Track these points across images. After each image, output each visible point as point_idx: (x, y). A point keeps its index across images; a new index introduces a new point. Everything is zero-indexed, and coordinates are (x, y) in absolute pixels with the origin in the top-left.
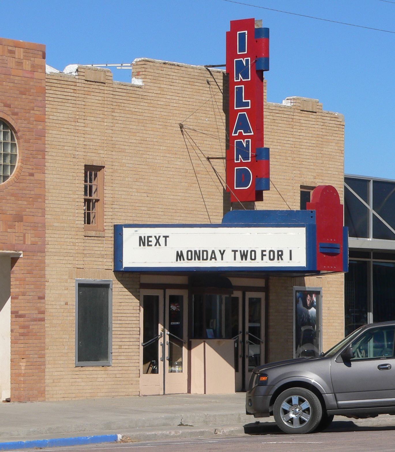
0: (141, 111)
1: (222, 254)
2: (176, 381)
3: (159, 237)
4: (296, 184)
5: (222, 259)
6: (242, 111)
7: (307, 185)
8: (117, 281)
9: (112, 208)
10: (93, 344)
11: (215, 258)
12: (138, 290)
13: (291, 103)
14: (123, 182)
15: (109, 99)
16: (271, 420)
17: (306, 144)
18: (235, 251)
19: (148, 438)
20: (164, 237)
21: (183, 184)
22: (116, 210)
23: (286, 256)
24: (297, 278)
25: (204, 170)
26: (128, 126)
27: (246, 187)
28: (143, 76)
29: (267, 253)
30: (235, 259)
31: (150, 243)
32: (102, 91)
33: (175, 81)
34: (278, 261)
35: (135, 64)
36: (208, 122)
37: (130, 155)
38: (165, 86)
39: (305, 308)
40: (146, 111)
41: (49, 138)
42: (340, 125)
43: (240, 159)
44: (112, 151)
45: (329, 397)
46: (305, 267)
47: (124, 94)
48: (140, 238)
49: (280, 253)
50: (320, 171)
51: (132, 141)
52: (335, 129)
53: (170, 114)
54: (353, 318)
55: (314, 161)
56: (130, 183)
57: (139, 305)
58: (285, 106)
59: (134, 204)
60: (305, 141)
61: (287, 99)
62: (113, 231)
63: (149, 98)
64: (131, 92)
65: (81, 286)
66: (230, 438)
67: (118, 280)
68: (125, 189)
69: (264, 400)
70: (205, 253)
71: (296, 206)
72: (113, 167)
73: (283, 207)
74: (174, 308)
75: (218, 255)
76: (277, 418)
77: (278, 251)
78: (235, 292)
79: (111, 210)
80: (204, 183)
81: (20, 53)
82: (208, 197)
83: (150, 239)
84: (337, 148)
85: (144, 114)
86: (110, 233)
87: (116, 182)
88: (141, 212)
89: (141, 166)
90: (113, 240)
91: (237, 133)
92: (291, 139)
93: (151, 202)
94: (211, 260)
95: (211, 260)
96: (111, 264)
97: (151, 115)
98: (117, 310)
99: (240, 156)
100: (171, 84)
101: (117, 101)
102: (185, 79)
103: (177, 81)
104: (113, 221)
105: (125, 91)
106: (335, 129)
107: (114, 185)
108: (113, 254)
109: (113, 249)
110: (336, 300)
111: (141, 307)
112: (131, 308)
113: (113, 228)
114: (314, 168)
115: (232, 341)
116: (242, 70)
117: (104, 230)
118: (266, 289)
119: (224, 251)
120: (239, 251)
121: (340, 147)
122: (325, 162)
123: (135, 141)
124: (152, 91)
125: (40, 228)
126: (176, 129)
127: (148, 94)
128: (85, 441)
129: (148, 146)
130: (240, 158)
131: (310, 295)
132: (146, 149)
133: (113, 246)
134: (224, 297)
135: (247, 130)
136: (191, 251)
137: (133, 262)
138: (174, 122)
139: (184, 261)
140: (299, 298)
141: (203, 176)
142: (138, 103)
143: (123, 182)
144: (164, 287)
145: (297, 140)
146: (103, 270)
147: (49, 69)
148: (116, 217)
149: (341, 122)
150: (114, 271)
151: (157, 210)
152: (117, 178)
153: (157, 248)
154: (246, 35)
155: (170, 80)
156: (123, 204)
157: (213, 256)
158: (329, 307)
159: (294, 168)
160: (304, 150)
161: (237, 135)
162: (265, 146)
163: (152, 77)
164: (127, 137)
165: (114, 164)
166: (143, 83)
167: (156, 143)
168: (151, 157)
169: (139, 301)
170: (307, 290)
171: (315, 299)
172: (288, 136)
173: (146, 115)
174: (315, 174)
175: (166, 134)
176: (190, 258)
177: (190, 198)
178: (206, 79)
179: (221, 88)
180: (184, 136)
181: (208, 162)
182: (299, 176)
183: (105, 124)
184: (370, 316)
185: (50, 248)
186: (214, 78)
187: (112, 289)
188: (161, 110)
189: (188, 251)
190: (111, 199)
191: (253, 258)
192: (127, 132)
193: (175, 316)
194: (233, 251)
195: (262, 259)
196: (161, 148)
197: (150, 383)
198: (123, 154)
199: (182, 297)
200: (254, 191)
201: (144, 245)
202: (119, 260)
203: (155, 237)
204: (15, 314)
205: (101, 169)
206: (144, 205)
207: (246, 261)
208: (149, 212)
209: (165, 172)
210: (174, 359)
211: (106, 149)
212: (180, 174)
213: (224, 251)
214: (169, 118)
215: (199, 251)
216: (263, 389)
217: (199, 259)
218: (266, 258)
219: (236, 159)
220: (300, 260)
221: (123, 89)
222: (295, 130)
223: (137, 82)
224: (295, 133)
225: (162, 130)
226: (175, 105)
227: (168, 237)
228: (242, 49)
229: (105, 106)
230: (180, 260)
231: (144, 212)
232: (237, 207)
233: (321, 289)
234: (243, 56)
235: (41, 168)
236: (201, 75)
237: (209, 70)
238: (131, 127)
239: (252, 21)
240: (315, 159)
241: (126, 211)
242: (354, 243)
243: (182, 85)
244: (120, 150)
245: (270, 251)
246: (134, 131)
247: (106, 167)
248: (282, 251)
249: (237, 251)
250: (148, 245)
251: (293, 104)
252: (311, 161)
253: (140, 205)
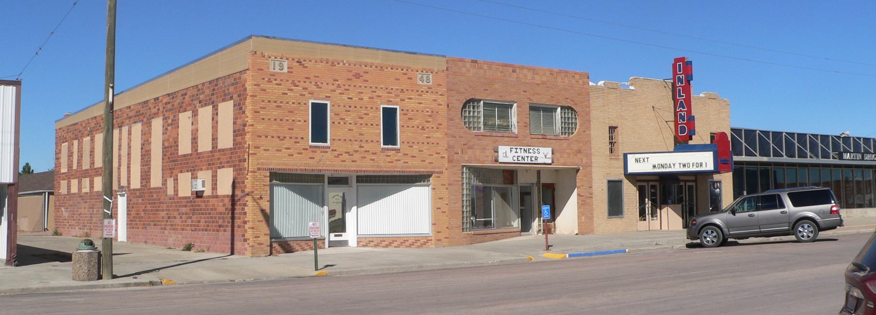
2: (655, 224)
6: (681, 99)
10: (615, 207)
16: (699, 241)
19: (640, 250)
23: (704, 165)
41: (592, 115)
45: (725, 230)
54: (737, 193)
65: (609, 182)
66: (680, 250)
69: (697, 234)
71: (709, 142)
73: (702, 143)
76: (702, 241)
81: (577, 77)
86: (622, 157)
115: (680, 206)
116: (680, 80)
118: (695, 181)
125: (589, 156)
128: (611, 253)
144: (648, 181)
147: (591, 84)
184: (745, 193)
185: (594, 165)
193: (654, 194)
197: (643, 225)
204: (579, 195)
210: (653, 214)
216: (694, 227)
220: (710, 167)
223: (632, 88)
232: (680, 143)
235: (589, 128)
239: (684, 58)
242: (736, 158)
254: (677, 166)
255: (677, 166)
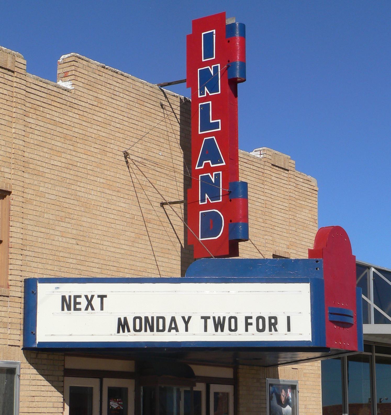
0: (68, 123)
1: (187, 323)
3: (92, 296)
4: (268, 252)
5: (187, 330)
7: (281, 255)
8: (28, 365)
9: (22, 255)
11: (176, 329)
12: (61, 378)
13: (261, 154)
14: (41, 219)
15: (19, 96)
17: (278, 206)
18: (206, 318)
20: (99, 296)
21: (129, 233)
22: (28, 258)
23: (282, 325)
24: (270, 368)
25: (156, 218)
26: (48, 141)
27: (216, 236)
28: (73, 77)
29: (253, 321)
30: (206, 330)
31: (78, 306)
32: (9, 83)
33: (118, 93)
34: (271, 333)
35: (62, 63)
36: (162, 157)
37: (52, 182)
38: (104, 98)
39: (279, 406)
40: (76, 125)
42: (312, 189)
43: (206, 200)
44: (23, 172)
46: (310, 341)
47: (44, 95)
48: (64, 298)
49: (273, 321)
50: (294, 240)
51: (55, 163)
52: (309, 193)
53: (112, 137)
55: (287, 227)
56: (51, 222)
57: (62, 401)
58: (254, 156)
59: (56, 252)
60: (277, 202)
61: (255, 151)
62: (23, 289)
63: (81, 108)
64: (53, 93)
67: (30, 363)
68: (43, 230)
70: (161, 321)
72: (25, 195)
74: (114, 405)
75: (181, 324)
77: (270, 318)
78: (198, 384)
79: (21, 257)
80: (157, 236)
82: (162, 255)
83: (78, 300)
84: (310, 216)
85: (74, 129)
86: (18, 291)
87: (29, 217)
88: (68, 265)
89: (68, 201)
90: (23, 302)
91: (202, 166)
92: (262, 197)
93: (83, 253)
94: (169, 331)
95: (169, 331)
96: (17, 337)
97: (84, 132)
98: (28, 407)
99: (206, 195)
100: (113, 96)
101: (32, 101)
102: (132, 95)
103: (121, 95)
104: (23, 274)
105: (46, 91)
106: (309, 193)
107: (26, 222)
108: (22, 323)
109: (22, 316)
110: (313, 396)
111: (65, 404)
112: (51, 405)
113: (23, 284)
114: (288, 235)
117: (8, 286)
119: (190, 318)
120: (212, 318)
121: (313, 215)
122: (298, 230)
123: (59, 164)
124: (85, 100)
126: (120, 158)
127: (80, 103)
129: (79, 174)
130: (207, 199)
131: (284, 390)
132: (75, 178)
133: (22, 312)
134: (182, 390)
135: (216, 160)
136: (140, 318)
137: (52, 335)
138: (116, 148)
139: (129, 333)
140: (273, 394)
141: (155, 227)
142: (65, 112)
143: (41, 219)
144: (100, 375)
145: (268, 199)
146: (5, 346)
148: (28, 269)
149: (314, 186)
150: (22, 349)
151: (92, 264)
152: (31, 212)
153: (88, 313)
154: (214, 36)
155: (111, 91)
156: (40, 250)
157: (173, 326)
158: (306, 405)
159: (266, 233)
160: (276, 213)
161: (202, 167)
162: (241, 179)
163: (86, 82)
164: (47, 155)
165: (26, 190)
166: (72, 87)
167: (90, 172)
168: (83, 190)
169: (63, 395)
170: (281, 383)
171: (290, 395)
172: (258, 192)
173: (76, 130)
174: (288, 244)
175: (105, 162)
176: (138, 328)
177: (138, 253)
178: (159, 101)
179: (178, 117)
180: (130, 169)
181: (162, 210)
182: (271, 242)
183: (13, 131)
186: (169, 102)
187: (19, 376)
188: (99, 128)
189: (135, 318)
190: (20, 241)
191: (233, 327)
192: (47, 149)
194: (202, 318)
195: (247, 330)
196: (98, 180)
198: (41, 179)
199: (127, 389)
200: (227, 243)
201: (69, 309)
202: (30, 332)
203: (86, 297)
205: (5, 196)
206: (72, 256)
207: (222, 333)
208: (79, 267)
209: (103, 214)
211: (13, 166)
212: (124, 219)
213: (190, 318)
214: (110, 141)
215: (153, 318)
217: (152, 330)
218: (252, 329)
219: (201, 200)
221: (42, 87)
222: (266, 187)
224: (266, 191)
225: (99, 156)
226: (118, 125)
227: (105, 296)
228: (208, 54)
229: (14, 104)
230: (124, 331)
231: (72, 266)
233: (297, 382)
234: (210, 63)
236: (152, 94)
237: (163, 91)
238: (53, 142)
240: (288, 224)
241: (44, 261)
243: (128, 102)
244: (36, 172)
245: (258, 318)
246: (58, 149)
247: (13, 193)
248: (275, 318)
249: (209, 318)
250: (75, 309)
251: (263, 156)
252: (284, 227)
253: (66, 255)
254: (196, 325)
255: (196, 325)
